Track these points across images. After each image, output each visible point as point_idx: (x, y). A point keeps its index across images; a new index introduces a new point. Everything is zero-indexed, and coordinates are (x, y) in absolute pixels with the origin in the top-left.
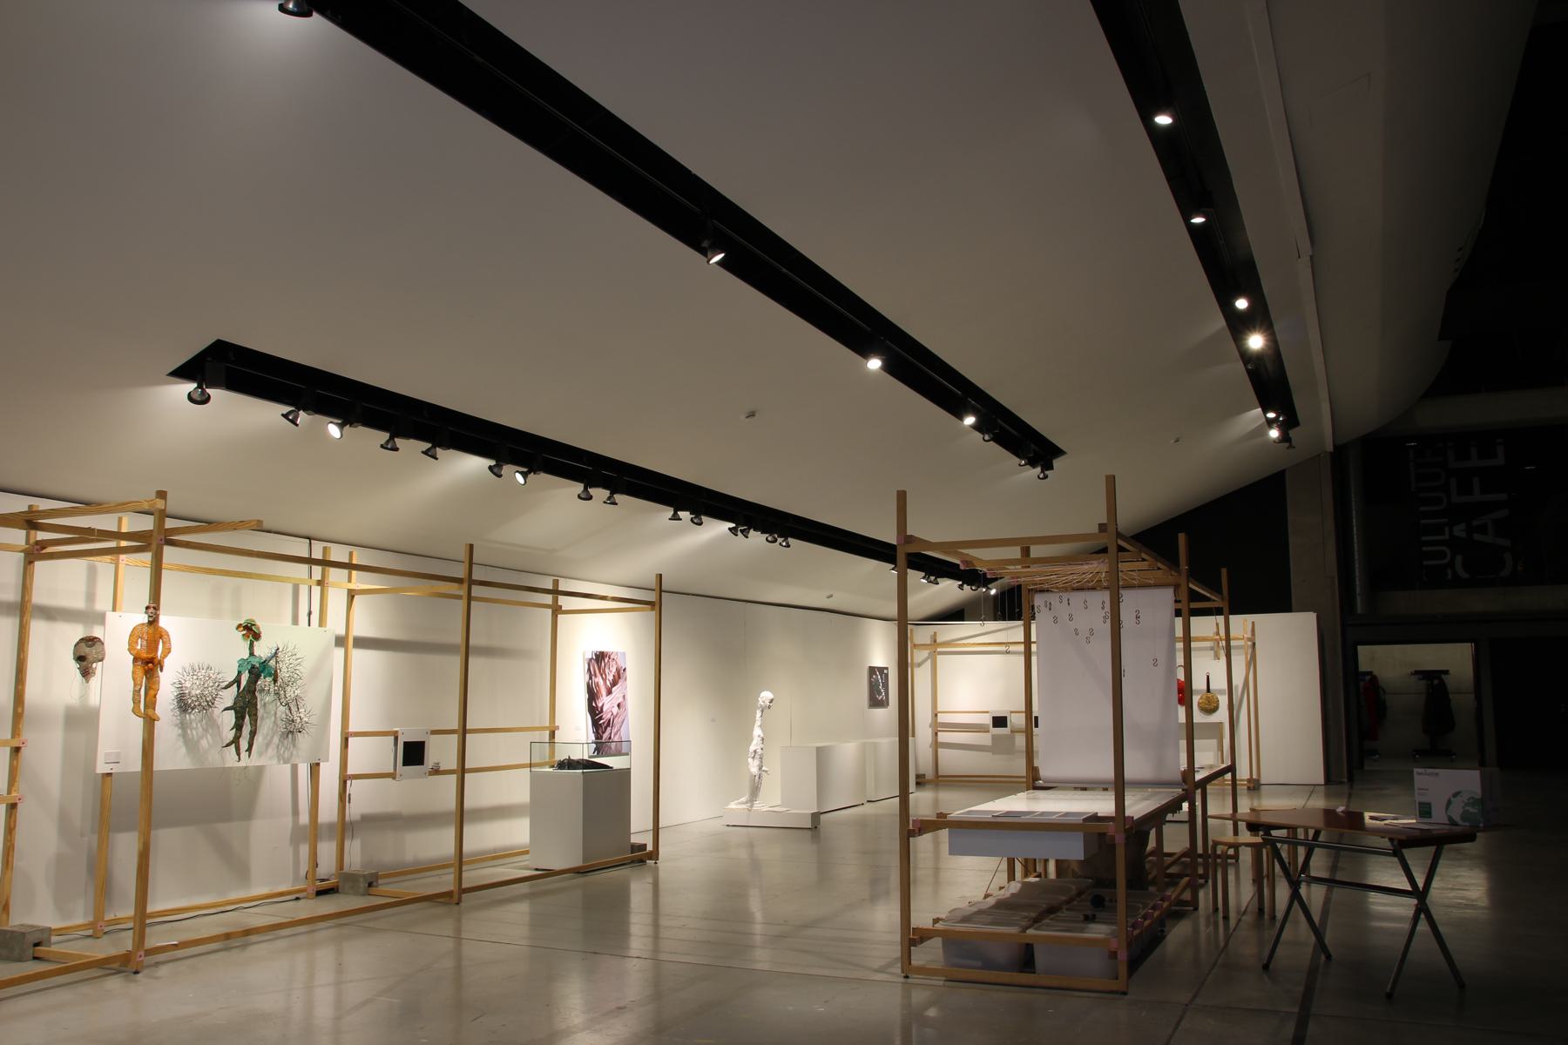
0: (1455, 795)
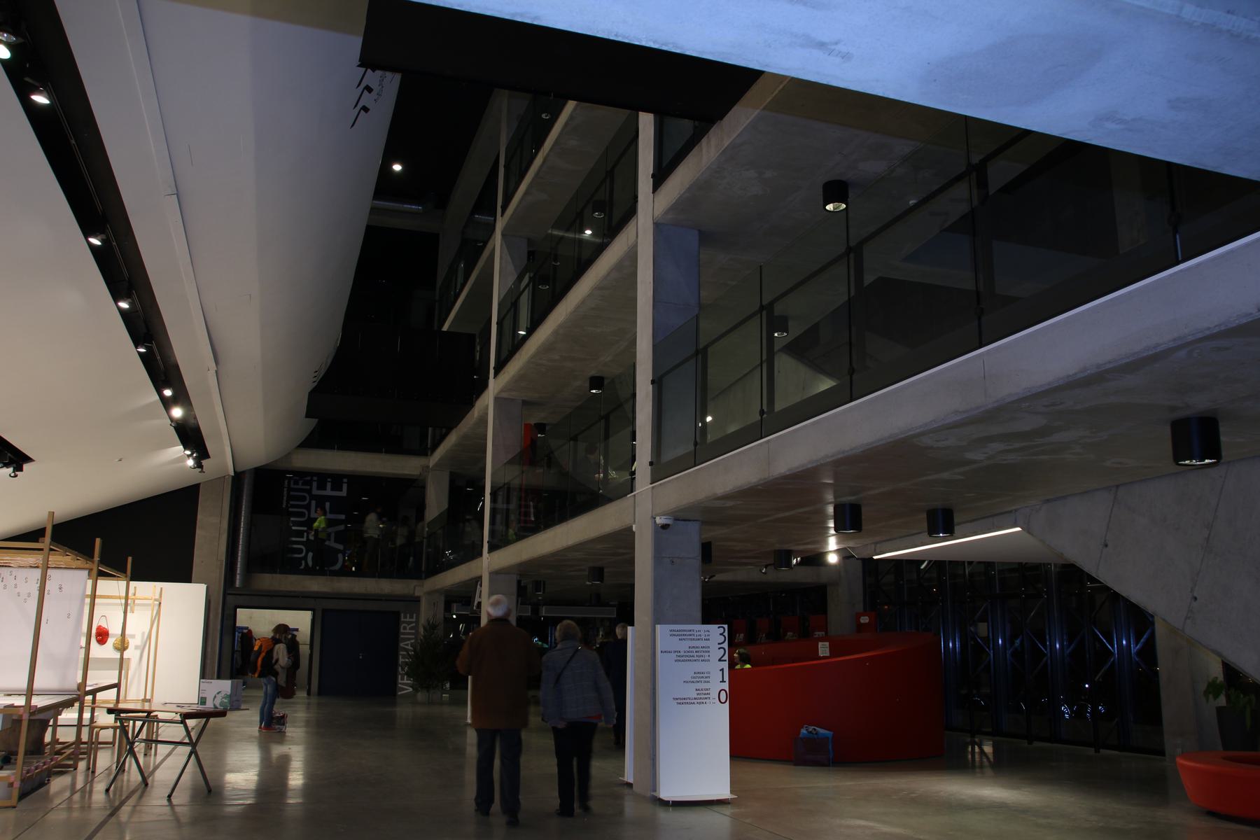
0: (218, 693)
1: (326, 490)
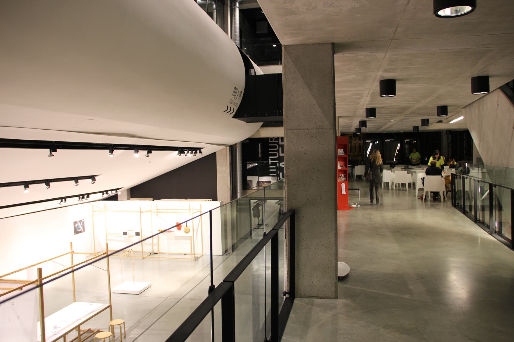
1: (283, 145)
